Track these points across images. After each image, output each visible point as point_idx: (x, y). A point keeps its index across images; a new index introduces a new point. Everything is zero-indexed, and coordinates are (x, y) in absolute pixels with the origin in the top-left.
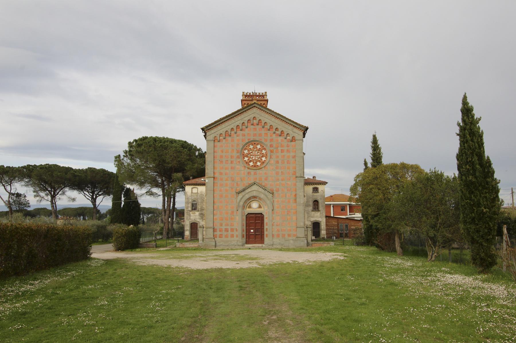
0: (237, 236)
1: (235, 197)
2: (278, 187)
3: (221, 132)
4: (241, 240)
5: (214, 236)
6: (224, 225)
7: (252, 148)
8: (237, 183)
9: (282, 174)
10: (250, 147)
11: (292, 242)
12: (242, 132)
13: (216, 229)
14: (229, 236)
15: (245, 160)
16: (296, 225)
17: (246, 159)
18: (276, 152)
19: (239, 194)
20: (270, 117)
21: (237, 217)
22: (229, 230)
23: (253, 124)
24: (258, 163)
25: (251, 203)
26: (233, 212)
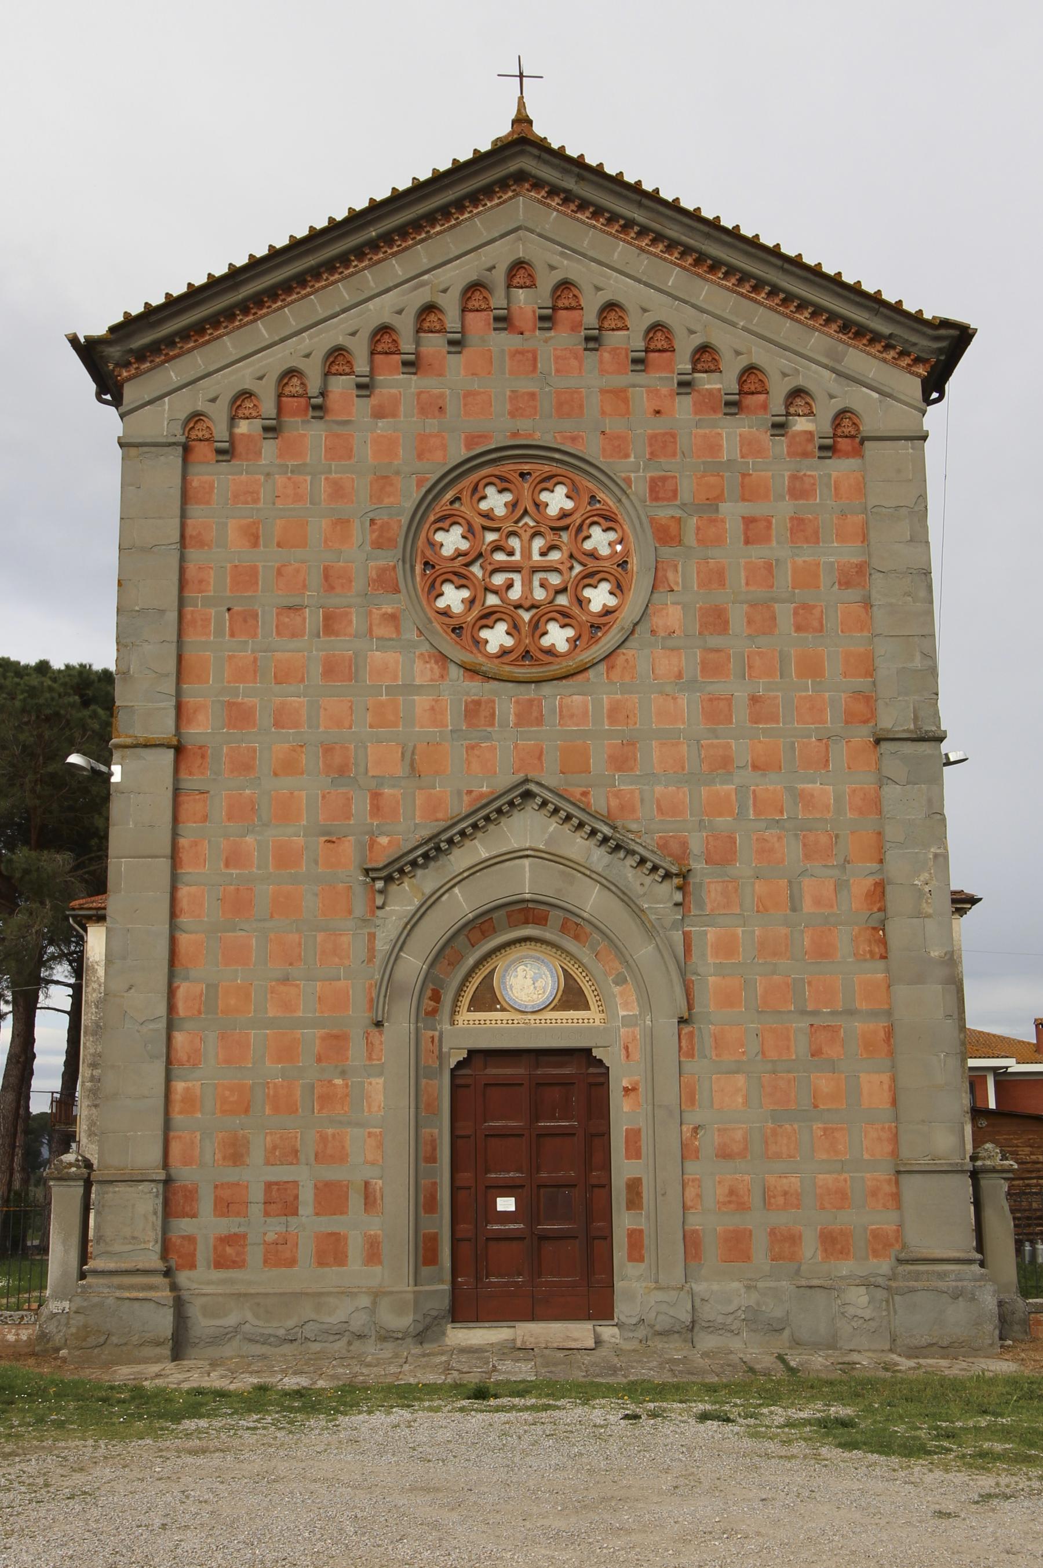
0: (373, 1253)
1: (360, 908)
2: (723, 822)
3: (243, 377)
4: (405, 1287)
5: (165, 1255)
6: (257, 1155)
7: (500, 511)
8: (376, 796)
9: (756, 719)
10: (484, 506)
11: (859, 1298)
12: (414, 383)
13: (191, 1194)
14: (306, 1250)
15: (441, 603)
16: (895, 1153)
17: (453, 598)
18: (700, 541)
19: (393, 888)
20: (645, 260)
21: (378, 1082)
22: (307, 1195)
23: (504, 321)
24: (553, 628)
25: (500, 963)
26: (337, 1042)
